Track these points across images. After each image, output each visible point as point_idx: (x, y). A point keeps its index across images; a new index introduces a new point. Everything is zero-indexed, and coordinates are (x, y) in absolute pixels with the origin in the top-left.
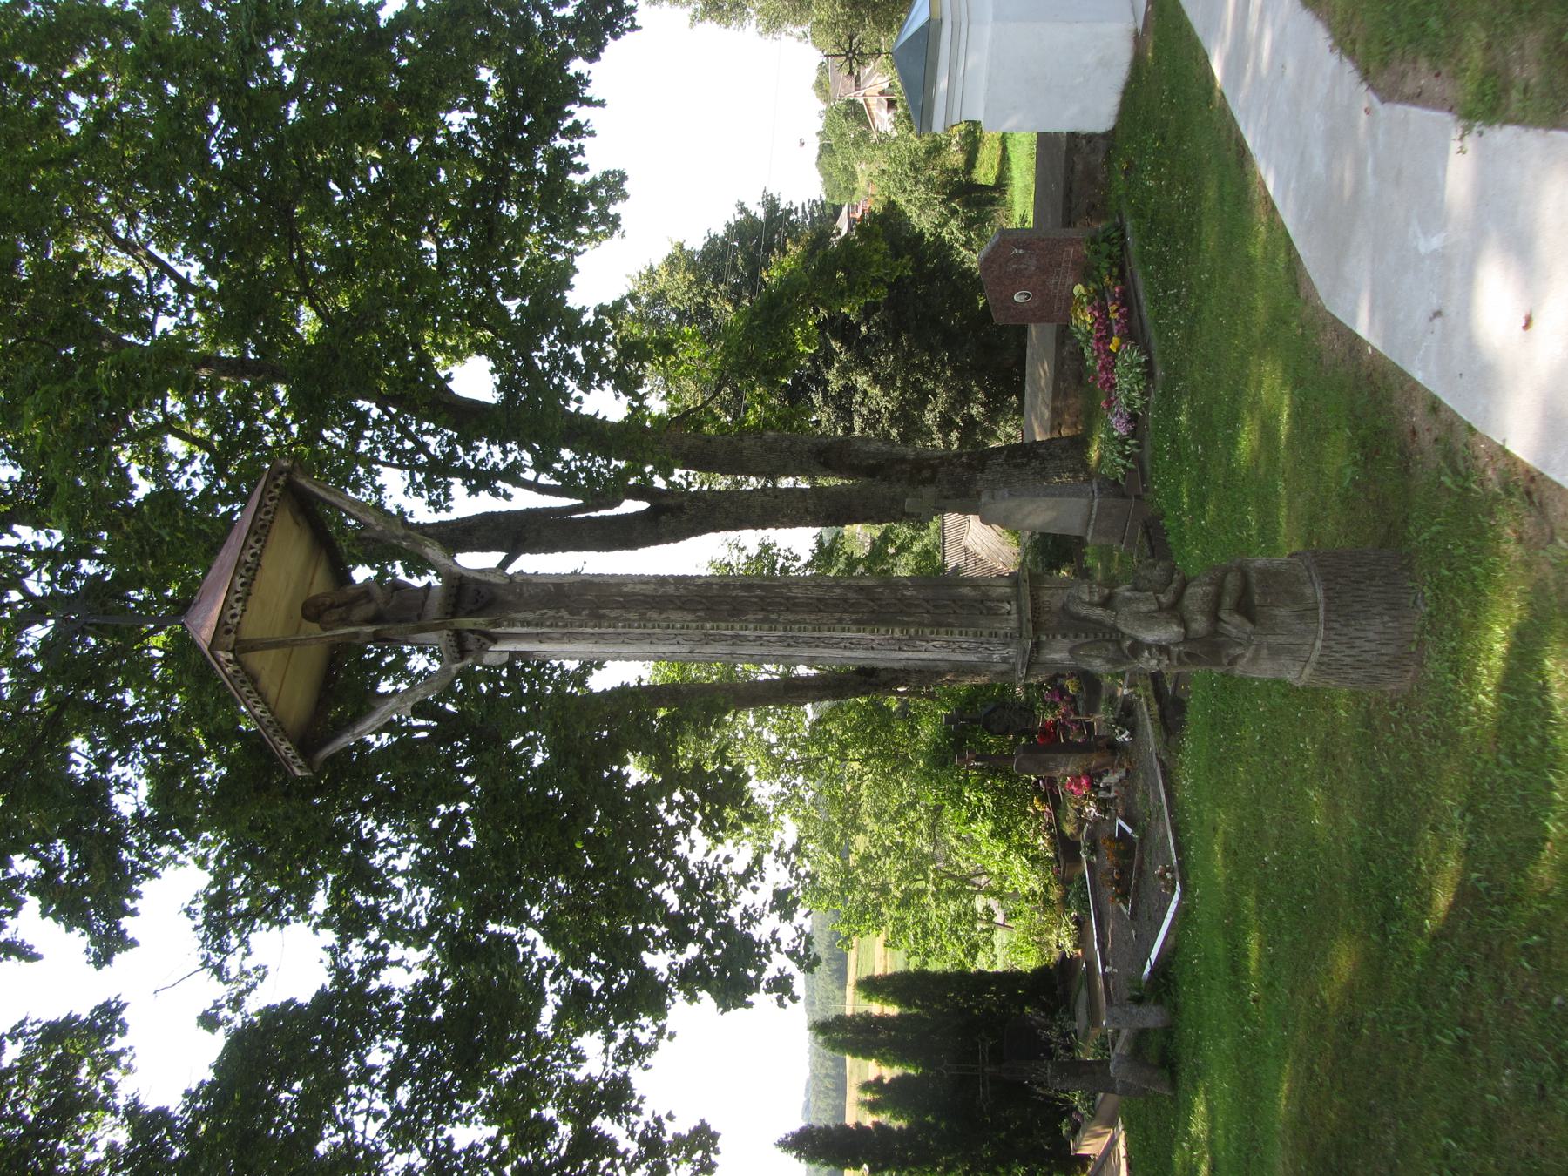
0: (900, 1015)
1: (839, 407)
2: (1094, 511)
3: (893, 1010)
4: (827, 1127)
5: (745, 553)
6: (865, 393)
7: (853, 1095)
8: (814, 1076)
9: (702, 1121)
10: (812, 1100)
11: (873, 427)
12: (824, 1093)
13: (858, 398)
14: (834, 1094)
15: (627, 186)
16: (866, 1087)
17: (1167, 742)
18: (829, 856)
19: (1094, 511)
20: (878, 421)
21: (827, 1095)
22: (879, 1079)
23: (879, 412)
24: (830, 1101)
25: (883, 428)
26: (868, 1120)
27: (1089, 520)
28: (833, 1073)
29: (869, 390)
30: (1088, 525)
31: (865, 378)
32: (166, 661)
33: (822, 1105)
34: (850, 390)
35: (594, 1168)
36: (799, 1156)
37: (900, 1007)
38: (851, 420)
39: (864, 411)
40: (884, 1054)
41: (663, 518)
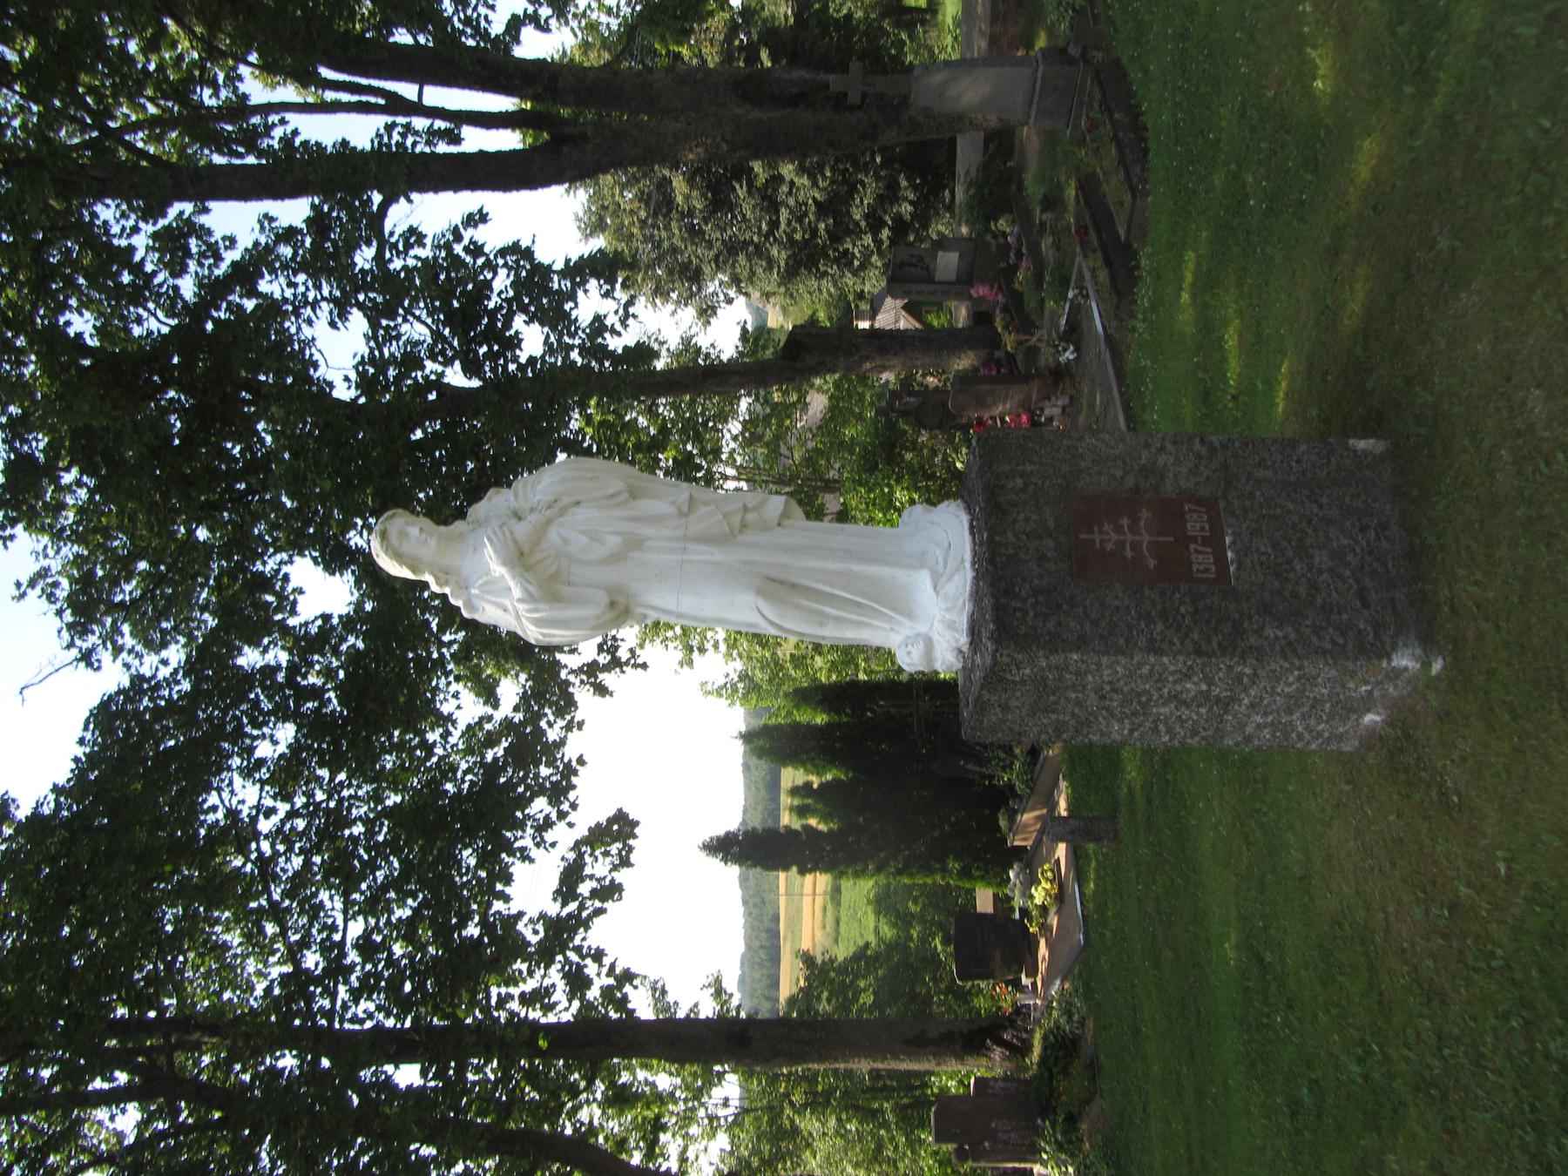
0: (829, 725)
1: (764, 198)
2: (1038, 85)
3: (820, 719)
4: (754, 829)
5: (665, 346)
6: (792, 183)
7: (785, 800)
8: (749, 947)
9: (632, 865)
10: (747, 971)
11: (800, 220)
12: (759, 964)
13: (785, 188)
14: (769, 964)
15: (637, 831)
16: (795, 791)
17: (1118, 307)
18: (758, 648)
19: (1038, 85)
20: (806, 214)
21: (761, 965)
22: (808, 785)
23: (806, 204)
24: (765, 971)
25: (810, 223)
26: (796, 824)
27: (1033, 97)
28: (767, 944)
29: (796, 180)
30: (1031, 103)
31: (791, 167)
32: (81, 511)
33: (757, 975)
34: (777, 180)
35: (571, 1172)
36: (725, 860)
37: (829, 714)
38: (777, 212)
39: (791, 202)
40: (813, 759)
41: (565, 149)
